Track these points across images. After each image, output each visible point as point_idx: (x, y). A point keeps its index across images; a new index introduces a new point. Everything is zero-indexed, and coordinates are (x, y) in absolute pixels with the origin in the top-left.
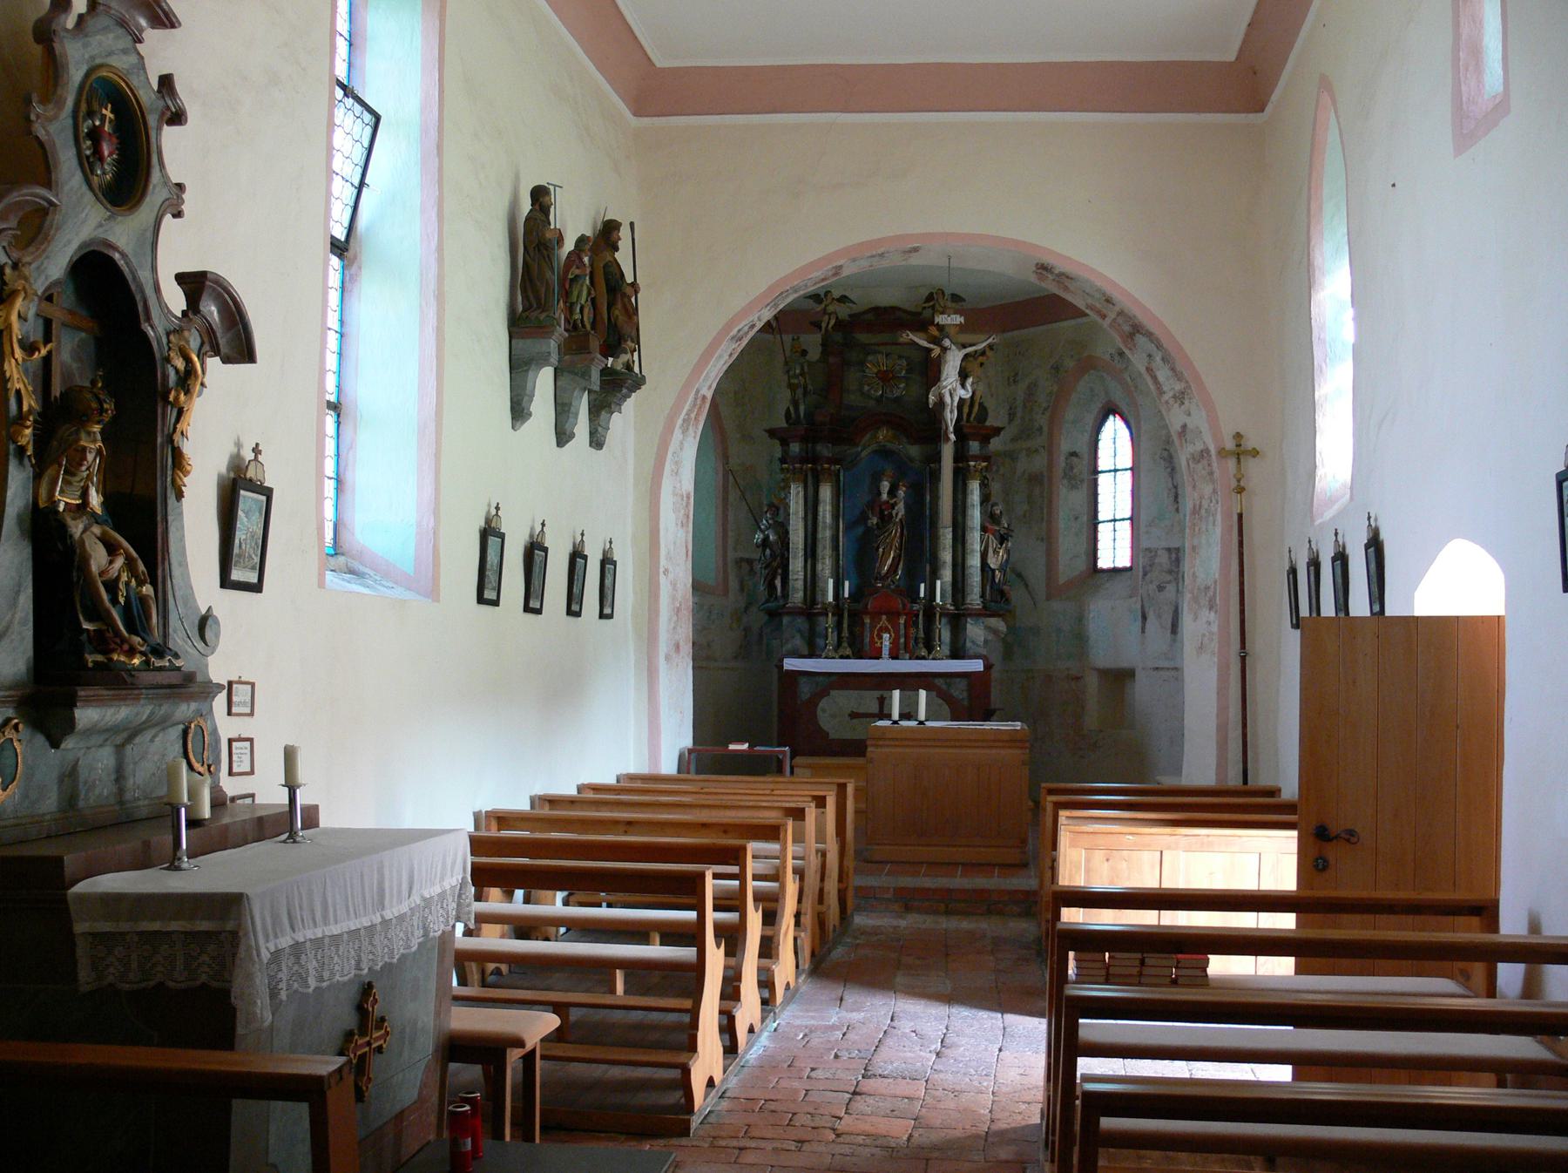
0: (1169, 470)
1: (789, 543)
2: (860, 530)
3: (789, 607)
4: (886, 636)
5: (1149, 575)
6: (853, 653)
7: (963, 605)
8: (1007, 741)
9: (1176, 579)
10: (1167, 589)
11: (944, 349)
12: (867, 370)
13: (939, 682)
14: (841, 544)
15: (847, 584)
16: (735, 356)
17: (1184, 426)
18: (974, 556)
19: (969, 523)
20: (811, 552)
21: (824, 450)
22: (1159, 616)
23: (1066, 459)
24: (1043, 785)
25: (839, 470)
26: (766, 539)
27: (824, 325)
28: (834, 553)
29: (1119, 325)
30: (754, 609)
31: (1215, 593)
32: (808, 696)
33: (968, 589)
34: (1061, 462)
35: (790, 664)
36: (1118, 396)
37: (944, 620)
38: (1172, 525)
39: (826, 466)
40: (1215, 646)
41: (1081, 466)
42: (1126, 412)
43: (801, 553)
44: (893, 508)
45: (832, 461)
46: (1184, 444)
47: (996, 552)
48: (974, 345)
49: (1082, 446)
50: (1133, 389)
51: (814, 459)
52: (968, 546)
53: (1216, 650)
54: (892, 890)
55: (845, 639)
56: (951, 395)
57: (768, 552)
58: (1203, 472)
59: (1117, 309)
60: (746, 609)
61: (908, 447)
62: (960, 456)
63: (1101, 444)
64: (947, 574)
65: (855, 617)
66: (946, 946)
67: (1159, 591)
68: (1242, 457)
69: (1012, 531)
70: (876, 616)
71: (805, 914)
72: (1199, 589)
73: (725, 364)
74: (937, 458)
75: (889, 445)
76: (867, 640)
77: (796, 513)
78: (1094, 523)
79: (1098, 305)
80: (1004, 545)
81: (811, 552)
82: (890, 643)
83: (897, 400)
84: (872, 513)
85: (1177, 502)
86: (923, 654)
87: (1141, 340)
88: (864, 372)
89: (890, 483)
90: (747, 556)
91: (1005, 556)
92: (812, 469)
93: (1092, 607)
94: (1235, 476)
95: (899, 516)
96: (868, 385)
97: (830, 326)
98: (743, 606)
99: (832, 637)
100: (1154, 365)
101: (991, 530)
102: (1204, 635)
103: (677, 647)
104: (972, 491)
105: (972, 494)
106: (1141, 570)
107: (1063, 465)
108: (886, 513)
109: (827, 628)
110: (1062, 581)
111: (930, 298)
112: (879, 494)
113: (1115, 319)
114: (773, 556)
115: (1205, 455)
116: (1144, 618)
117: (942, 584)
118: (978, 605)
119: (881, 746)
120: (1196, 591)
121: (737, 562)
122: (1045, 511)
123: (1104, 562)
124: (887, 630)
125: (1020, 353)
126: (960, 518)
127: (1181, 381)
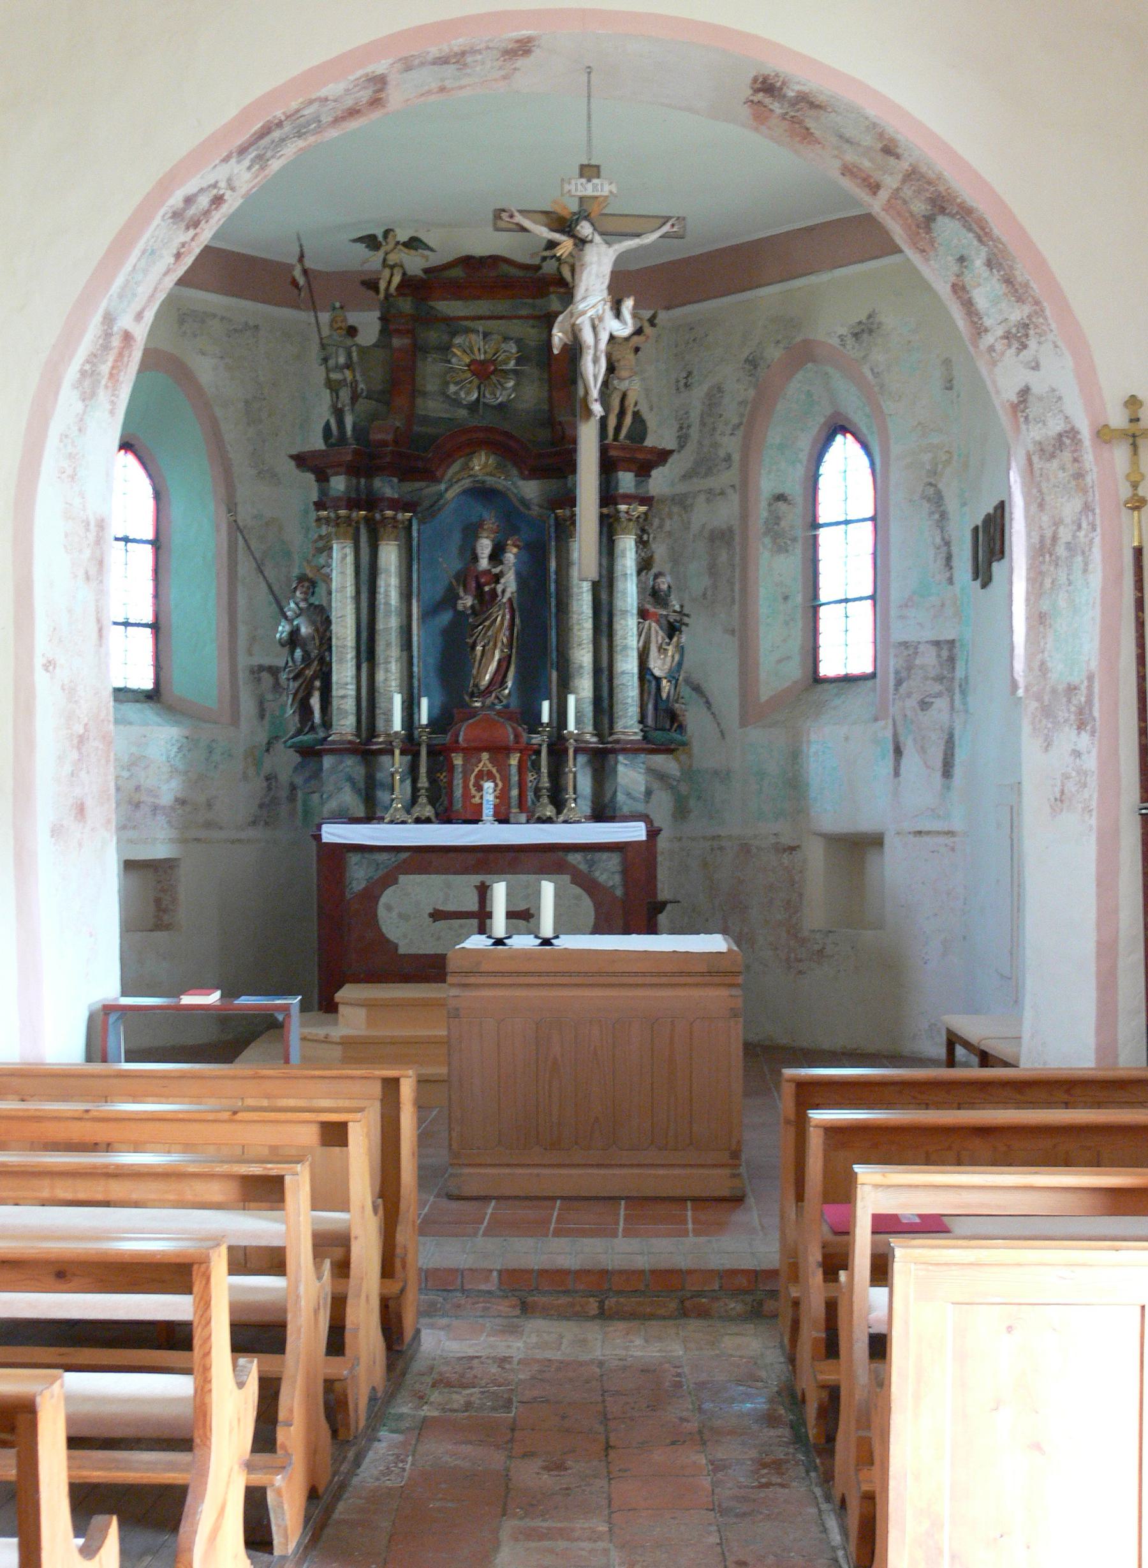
0: (937, 516)
1: (330, 639)
2: (446, 617)
3: (334, 742)
4: (488, 786)
5: (905, 685)
6: (437, 815)
7: (611, 734)
8: (702, 974)
9: (950, 691)
10: (935, 706)
11: (581, 243)
12: (454, 360)
13: (575, 858)
14: (415, 639)
15: (424, 702)
16: (189, 261)
17: (1025, 392)
18: (627, 656)
19: (619, 604)
20: (367, 653)
21: (387, 487)
22: (923, 750)
23: (770, 505)
24: (789, 1072)
25: (410, 521)
26: (294, 633)
27: (382, 285)
28: (405, 653)
29: (905, 202)
30: (279, 746)
32: (363, 885)
33: (618, 709)
34: (761, 512)
35: (334, 833)
36: (854, 407)
37: (582, 759)
38: (943, 605)
39: (389, 513)
40: (1091, 793)
41: (793, 517)
42: (864, 430)
43: (351, 655)
44: (497, 582)
45: (396, 505)
46: (1023, 427)
47: (661, 649)
48: (638, 235)
49: (793, 483)
50: (876, 389)
51: (370, 502)
52: (618, 640)
53: (1094, 804)
54: (495, 1274)
55: (423, 791)
57: (298, 653)
58: (1061, 474)
59: (905, 165)
60: (269, 744)
61: (521, 483)
62: (608, 497)
63: (822, 482)
64: (584, 685)
65: (440, 756)
66: (605, 1418)
67: (922, 710)
68: (1141, 442)
69: (688, 616)
70: (471, 752)
71: (289, 1424)
72: (1054, 691)
73: (166, 273)
74: (569, 500)
75: (490, 480)
76: (458, 792)
78: (813, 608)
79: (866, 164)
80: (675, 639)
81: (367, 653)
82: (496, 797)
83: (501, 406)
84: (465, 591)
85: (951, 568)
86: (548, 814)
87: (947, 228)
88: (449, 362)
89: (493, 541)
90: (267, 661)
91: (677, 658)
92: (365, 517)
93: (813, 737)
94: (1128, 476)
95: (508, 595)
96: (456, 383)
98: (266, 741)
99: (402, 790)
100: (968, 279)
101: (655, 614)
102: (1066, 777)
103: (81, 810)
104: (624, 552)
105: (624, 556)
106: (892, 676)
107: (764, 514)
108: (487, 589)
109: (392, 775)
110: (764, 698)
112: (475, 558)
113: (898, 189)
114: (306, 657)
115: (1068, 442)
116: (898, 751)
117: (577, 701)
118: (635, 733)
119: (478, 986)
120: (1046, 698)
121: (252, 672)
122: (737, 587)
123: (828, 668)
124: (490, 776)
125: (694, 340)
126: (604, 596)
127: (1023, 302)
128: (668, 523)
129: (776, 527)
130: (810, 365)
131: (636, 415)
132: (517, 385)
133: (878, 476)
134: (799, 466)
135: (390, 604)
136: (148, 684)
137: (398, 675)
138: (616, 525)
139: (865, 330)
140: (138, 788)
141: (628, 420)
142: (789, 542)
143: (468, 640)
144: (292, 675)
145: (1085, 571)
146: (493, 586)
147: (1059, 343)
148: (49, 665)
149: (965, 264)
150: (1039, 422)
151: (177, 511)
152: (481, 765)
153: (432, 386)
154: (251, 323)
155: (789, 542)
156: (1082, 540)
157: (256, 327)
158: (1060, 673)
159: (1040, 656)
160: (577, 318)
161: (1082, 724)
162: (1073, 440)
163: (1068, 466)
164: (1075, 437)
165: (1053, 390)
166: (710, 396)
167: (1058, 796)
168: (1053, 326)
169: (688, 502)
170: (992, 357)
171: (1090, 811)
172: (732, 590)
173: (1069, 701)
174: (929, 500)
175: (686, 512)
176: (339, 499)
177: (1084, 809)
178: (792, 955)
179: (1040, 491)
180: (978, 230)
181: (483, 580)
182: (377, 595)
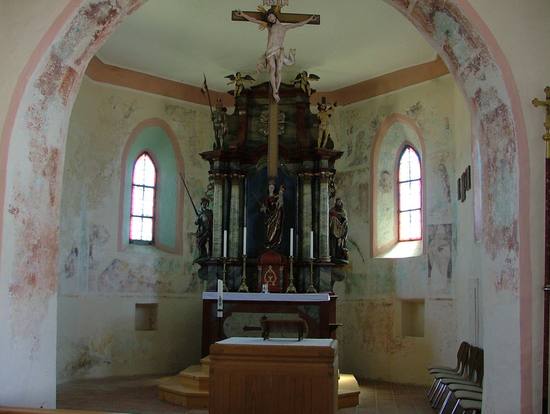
0: (444, 177)
9: (450, 243)
12: (262, 120)
13: (301, 308)
17: (479, 92)
21: (233, 165)
31: (515, 234)
34: (378, 177)
38: (447, 210)
41: (390, 180)
42: (417, 146)
44: (276, 201)
46: (479, 109)
48: (298, 22)
51: (228, 171)
53: (518, 285)
56: (276, 61)
58: (497, 128)
67: (439, 251)
70: (265, 265)
72: (496, 231)
77: (234, 212)
92: (227, 176)
95: (280, 206)
96: (262, 128)
97: (239, 93)
100: (450, 42)
108: (272, 204)
111: (299, 76)
116: (430, 267)
120: (493, 234)
126: (316, 207)
128: (344, 182)
129: (384, 183)
130: (395, 123)
131: (329, 139)
132: (285, 128)
133: (422, 162)
134: (392, 160)
135: (236, 209)
136: (150, 239)
137: (238, 236)
138: (321, 180)
139: (416, 109)
140: (142, 277)
141: (326, 141)
142: (389, 189)
143: (265, 223)
144: (198, 236)
145: (511, 171)
146: (275, 203)
147: (494, 64)
148: (14, 211)
149: (449, 34)
150: (486, 105)
151: (163, 175)
152: (269, 270)
153: (253, 129)
154: (193, 111)
155: (389, 189)
156: (509, 157)
157: (195, 112)
158: (498, 221)
159: (489, 215)
160: (267, 56)
161: (511, 246)
162: (502, 111)
163: (501, 123)
164: (503, 109)
165: (493, 88)
166: (359, 135)
167: (499, 281)
168: (492, 56)
169: (351, 174)
170: (463, 78)
171: (517, 289)
172: (368, 207)
173: (504, 235)
174: (441, 170)
175: (351, 178)
176: (217, 169)
177: (513, 287)
178: (389, 346)
179: (487, 138)
180: (454, 15)
181: (271, 201)
182: (231, 206)
